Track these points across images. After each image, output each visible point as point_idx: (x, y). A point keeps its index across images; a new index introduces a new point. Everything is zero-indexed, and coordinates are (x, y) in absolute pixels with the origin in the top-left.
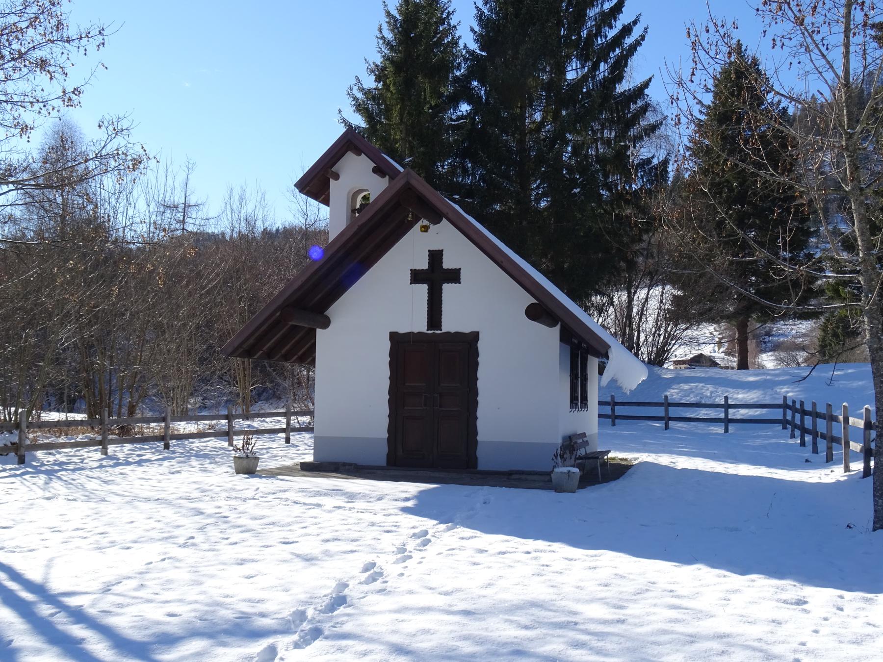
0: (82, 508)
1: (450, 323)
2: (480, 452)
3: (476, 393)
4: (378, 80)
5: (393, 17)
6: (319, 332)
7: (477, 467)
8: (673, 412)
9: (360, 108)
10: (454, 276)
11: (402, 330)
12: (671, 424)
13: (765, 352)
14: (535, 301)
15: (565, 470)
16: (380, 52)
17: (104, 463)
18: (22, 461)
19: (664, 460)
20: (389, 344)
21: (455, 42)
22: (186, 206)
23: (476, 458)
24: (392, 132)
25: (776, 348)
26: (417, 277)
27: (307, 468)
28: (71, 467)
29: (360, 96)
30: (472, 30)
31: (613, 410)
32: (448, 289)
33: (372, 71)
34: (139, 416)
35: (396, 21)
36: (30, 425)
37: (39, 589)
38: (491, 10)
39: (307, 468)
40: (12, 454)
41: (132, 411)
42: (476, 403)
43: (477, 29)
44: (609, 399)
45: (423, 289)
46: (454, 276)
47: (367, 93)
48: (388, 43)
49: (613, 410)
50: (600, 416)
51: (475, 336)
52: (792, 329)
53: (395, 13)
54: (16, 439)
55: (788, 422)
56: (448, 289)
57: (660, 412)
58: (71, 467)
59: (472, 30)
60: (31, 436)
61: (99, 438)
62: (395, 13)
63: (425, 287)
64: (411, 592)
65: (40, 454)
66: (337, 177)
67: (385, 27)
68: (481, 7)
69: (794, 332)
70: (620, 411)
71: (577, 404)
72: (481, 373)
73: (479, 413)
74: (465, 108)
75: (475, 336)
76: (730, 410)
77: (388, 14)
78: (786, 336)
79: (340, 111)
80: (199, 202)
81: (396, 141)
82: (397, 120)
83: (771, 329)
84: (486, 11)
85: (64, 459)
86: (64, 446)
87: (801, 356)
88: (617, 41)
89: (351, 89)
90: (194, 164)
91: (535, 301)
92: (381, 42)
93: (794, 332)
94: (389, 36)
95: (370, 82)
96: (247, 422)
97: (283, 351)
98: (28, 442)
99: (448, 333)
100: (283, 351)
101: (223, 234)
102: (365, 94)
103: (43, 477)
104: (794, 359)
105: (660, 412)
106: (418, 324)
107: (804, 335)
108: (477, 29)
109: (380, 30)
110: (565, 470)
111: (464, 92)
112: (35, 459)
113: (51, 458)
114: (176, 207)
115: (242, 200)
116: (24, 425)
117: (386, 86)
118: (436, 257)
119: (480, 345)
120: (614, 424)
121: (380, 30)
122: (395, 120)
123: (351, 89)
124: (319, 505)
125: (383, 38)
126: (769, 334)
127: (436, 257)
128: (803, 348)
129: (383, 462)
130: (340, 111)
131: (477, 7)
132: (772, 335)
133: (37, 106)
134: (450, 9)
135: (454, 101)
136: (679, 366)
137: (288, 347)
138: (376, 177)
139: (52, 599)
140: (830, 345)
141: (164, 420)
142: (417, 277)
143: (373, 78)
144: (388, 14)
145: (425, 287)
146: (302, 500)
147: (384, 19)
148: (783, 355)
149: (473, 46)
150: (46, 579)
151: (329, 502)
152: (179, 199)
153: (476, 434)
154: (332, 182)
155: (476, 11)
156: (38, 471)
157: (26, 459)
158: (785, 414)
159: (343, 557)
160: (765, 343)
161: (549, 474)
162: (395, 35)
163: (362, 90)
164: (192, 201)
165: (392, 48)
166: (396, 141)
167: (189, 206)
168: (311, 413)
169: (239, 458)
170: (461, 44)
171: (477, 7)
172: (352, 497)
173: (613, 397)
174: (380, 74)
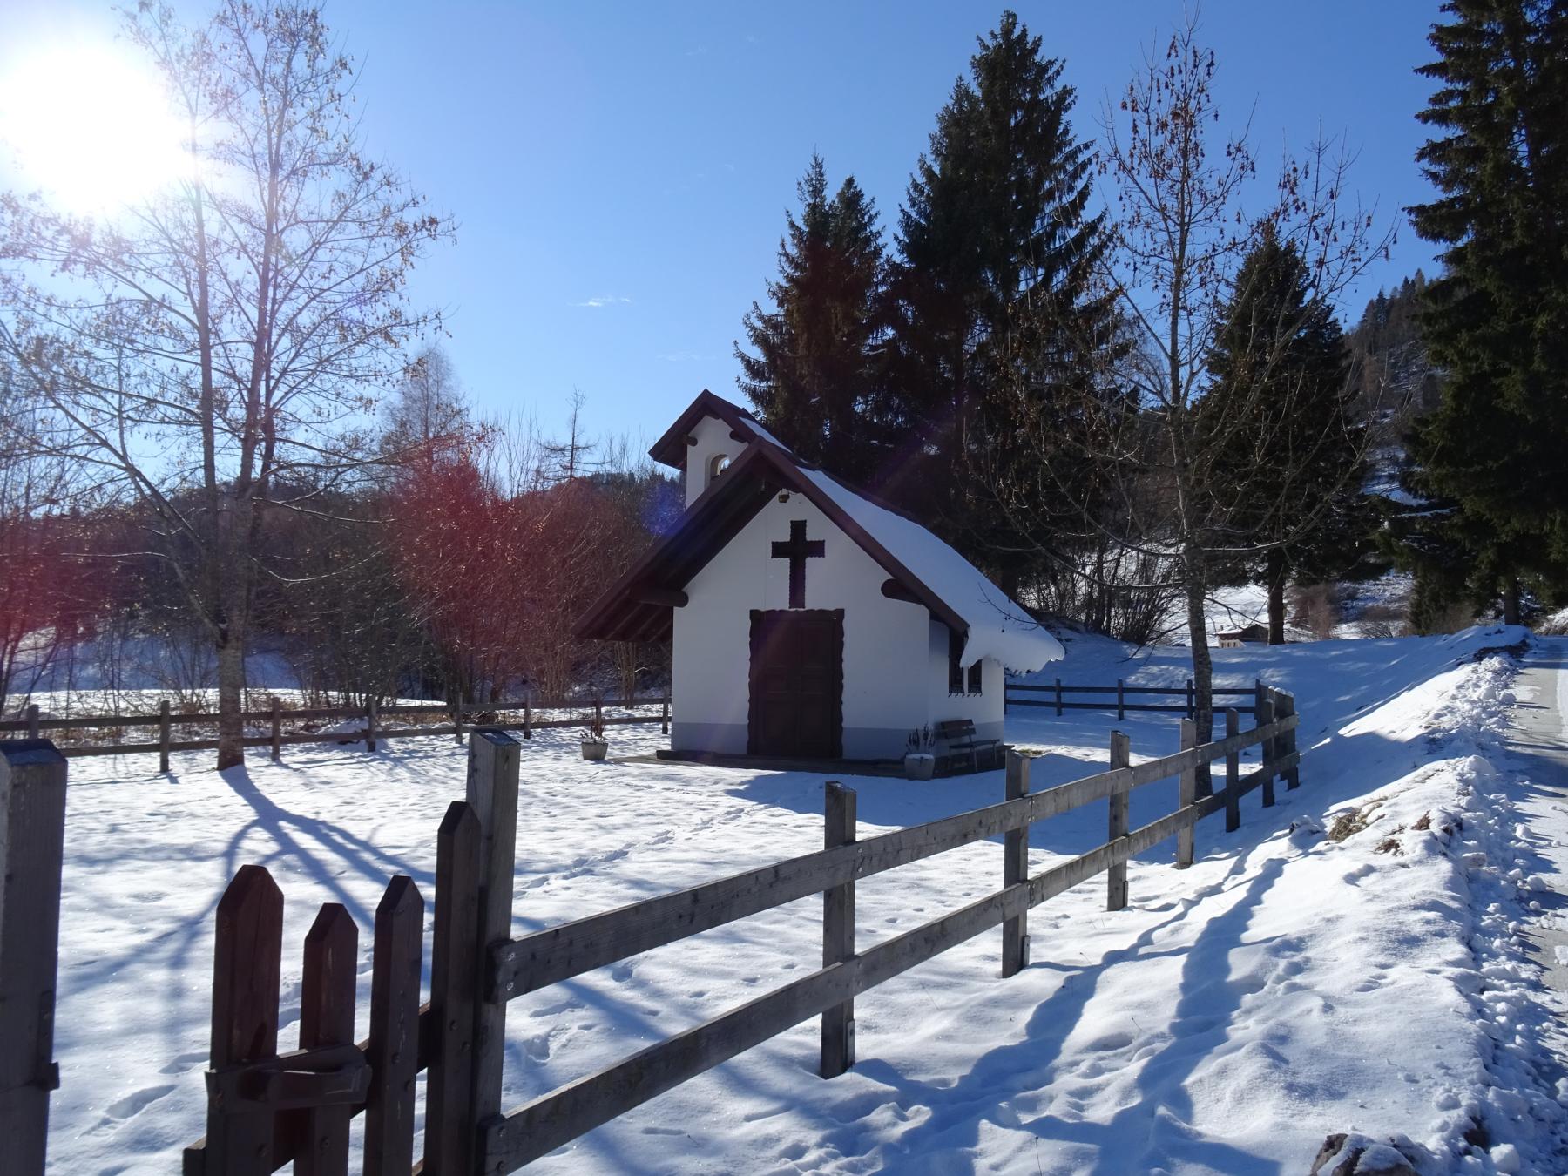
0: (416, 790)
1: (814, 600)
2: (844, 740)
3: (841, 676)
4: (780, 304)
5: (798, 229)
6: (676, 610)
7: (841, 754)
8: (1129, 699)
9: (760, 339)
10: (818, 549)
11: (763, 609)
12: (1127, 713)
13: (1346, 621)
14: (891, 577)
15: (917, 756)
16: (783, 271)
17: (457, 751)
18: (372, 748)
19: (1060, 750)
20: (749, 623)
21: (877, 253)
22: (574, 448)
23: (841, 746)
24: (798, 366)
25: (1360, 616)
26: (778, 550)
27: (663, 756)
28: (421, 755)
29: (759, 325)
30: (896, 238)
31: (1059, 697)
32: (811, 562)
33: (774, 294)
34: (503, 702)
35: (801, 234)
36: (381, 710)
37: (366, 846)
38: (919, 213)
39: (663, 756)
40: (363, 742)
41: (495, 695)
42: (841, 687)
43: (901, 237)
44: (1053, 684)
45: (785, 563)
46: (818, 549)
47: (769, 321)
48: (790, 260)
49: (1059, 697)
50: (1007, 701)
51: (840, 614)
52: (1385, 591)
53: (800, 223)
54: (366, 726)
55: (1193, 709)
56: (811, 562)
57: (1113, 699)
58: (421, 755)
59: (896, 238)
60: (383, 724)
61: (453, 724)
62: (800, 223)
63: (787, 561)
64: (628, 826)
65: (391, 742)
66: (694, 442)
67: (788, 240)
68: (907, 209)
69: (1388, 594)
70: (1051, 697)
71: (962, 691)
72: (846, 654)
73: (845, 697)
74: (890, 332)
75: (840, 614)
76: (1063, 694)
77: (792, 225)
78: (1376, 600)
79: (736, 343)
80: (590, 443)
81: (802, 377)
82: (804, 352)
83: (1356, 591)
84: (914, 215)
85: (416, 747)
86: (416, 733)
87: (1396, 627)
88: (1080, 242)
89: (748, 317)
90: (583, 397)
91: (891, 577)
92: (783, 259)
93: (1388, 594)
94: (793, 251)
95: (771, 308)
96: (629, 712)
97: (639, 632)
98: (380, 729)
99: (812, 611)
100: (639, 632)
101: (632, 475)
102: (764, 322)
103: (389, 764)
104: (1386, 630)
105: (1113, 699)
106: (780, 600)
107: (1401, 599)
108: (901, 237)
109: (783, 246)
110: (917, 756)
111: (886, 313)
112: (386, 746)
113: (402, 747)
114: (562, 450)
115: (623, 450)
116: (374, 710)
117: (789, 314)
118: (798, 528)
119: (846, 624)
120: (1059, 714)
121: (783, 246)
122: (801, 352)
123: (748, 317)
124: (650, 787)
125: (786, 255)
126: (1352, 596)
127: (798, 528)
128: (1395, 616)
129: (743, 750)
130: (736, 343)
131: (902, 211)
132: (1357, 599)
133: (381, 380)
134: (873, 212)
135: (876, 324)
136: (1226, 642)
137: (644, 626)
138: (735, 442)
139: (375, 851)
140: (1428, 612)
141: (523, 706)
142: (778, 550)
143: (775, 302)
144: (792, 225)
145: (787, 561)
146: (635, 783)
147: (787, 233)
148: (1369, 625)
149: (898, 258)
150: (370, 838)
151: (659, 785)
152: (564, 440)
153: (841, 720)
154: (690, 448)
155: (901, 215)
156: (385, 758)
157: (377, 747)
158: (1190, 701)
159: (713, 855)
160: (1347, 609)
161: (902, 762)
162: (801, 249)
163: (761, 317)
164: (581, 442)
165: (797, 266)
166: (802, 377)
167: (578, 448)
168: (666, 700)
169: (587, 744)
170: (885, 252)
171: (902, 211)
172: (687, 782)
173: (1058, 681)
174: (783, 297)
